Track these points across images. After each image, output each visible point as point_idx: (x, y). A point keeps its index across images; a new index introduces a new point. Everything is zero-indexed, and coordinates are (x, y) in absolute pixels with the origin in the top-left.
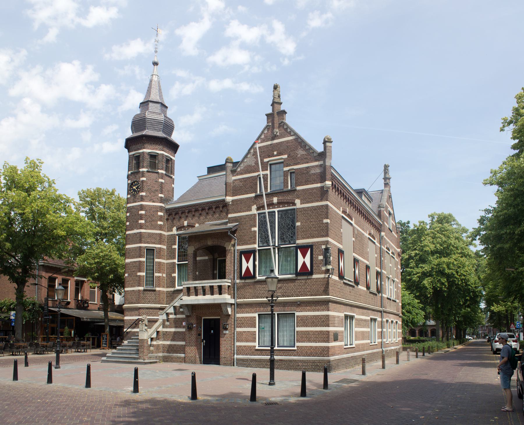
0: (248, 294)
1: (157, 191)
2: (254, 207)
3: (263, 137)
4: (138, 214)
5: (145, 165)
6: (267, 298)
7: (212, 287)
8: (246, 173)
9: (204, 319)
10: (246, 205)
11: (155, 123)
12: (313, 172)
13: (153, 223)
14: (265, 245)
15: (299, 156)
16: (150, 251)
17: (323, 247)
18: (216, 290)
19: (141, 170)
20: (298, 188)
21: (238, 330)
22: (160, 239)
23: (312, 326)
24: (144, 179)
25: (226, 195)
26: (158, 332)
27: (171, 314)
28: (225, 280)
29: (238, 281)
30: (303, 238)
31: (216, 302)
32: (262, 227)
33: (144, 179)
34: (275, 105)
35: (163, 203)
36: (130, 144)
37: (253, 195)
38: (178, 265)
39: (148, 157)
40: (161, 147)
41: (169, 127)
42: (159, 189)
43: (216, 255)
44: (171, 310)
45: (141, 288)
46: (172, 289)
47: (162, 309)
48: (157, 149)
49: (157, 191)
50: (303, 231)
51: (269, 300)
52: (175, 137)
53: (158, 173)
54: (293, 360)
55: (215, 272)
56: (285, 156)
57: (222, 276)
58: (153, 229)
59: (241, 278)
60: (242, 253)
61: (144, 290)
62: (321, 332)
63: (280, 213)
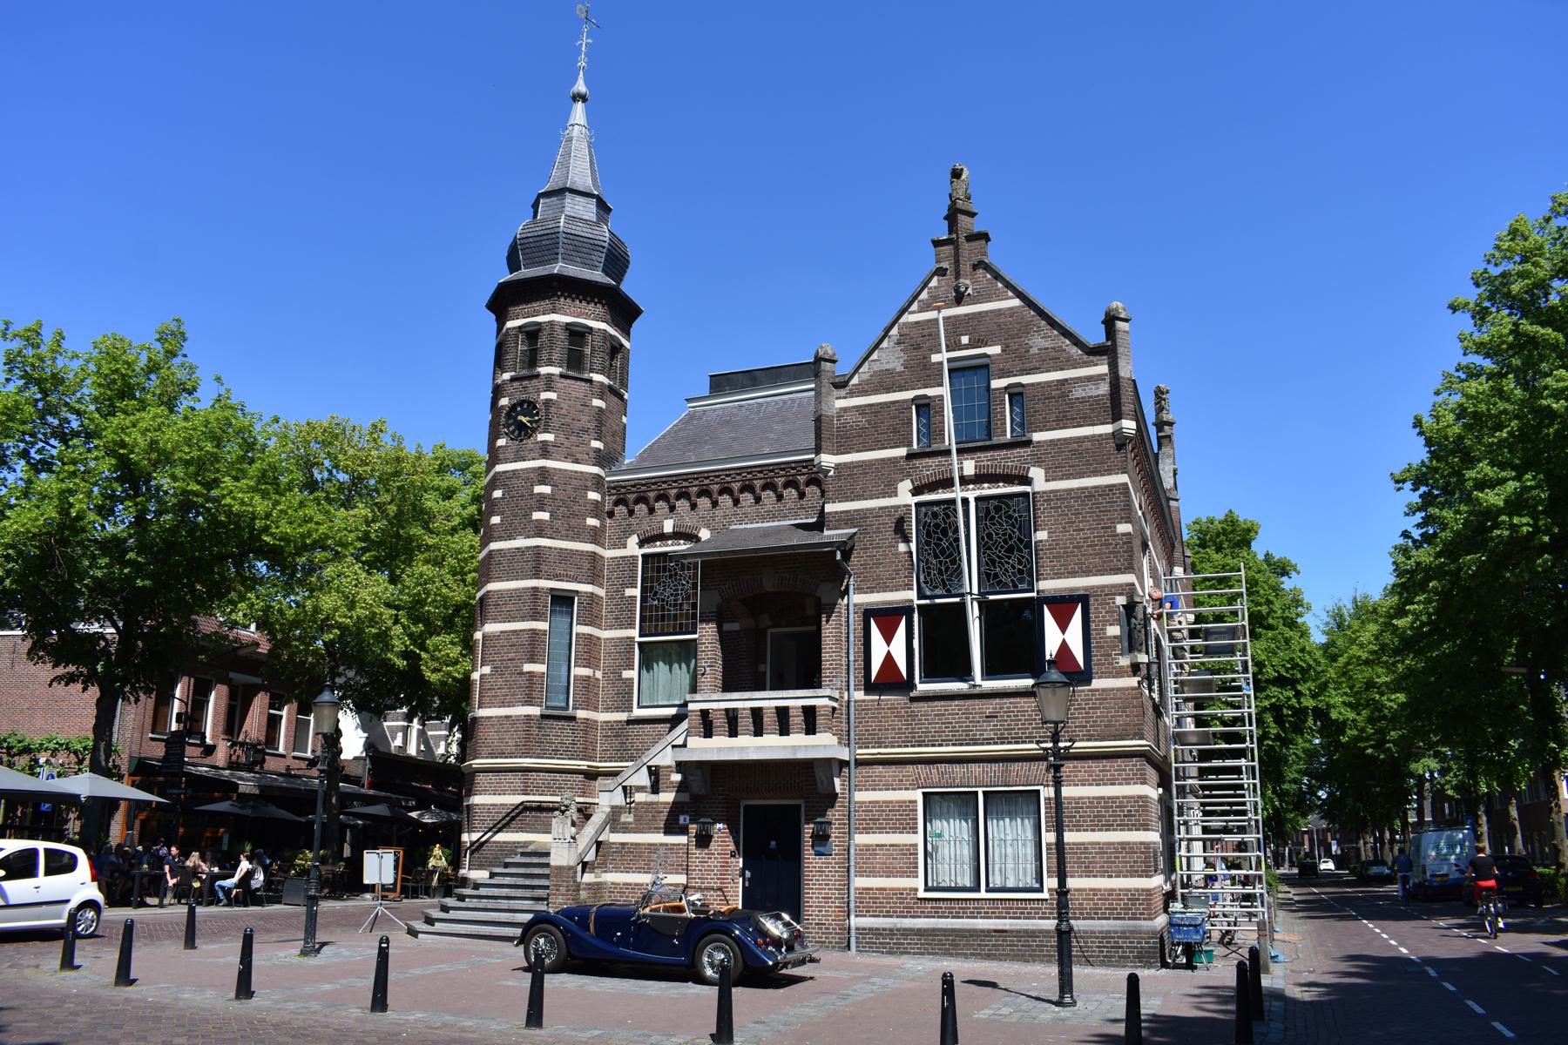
0: (891, 734)
1: (585, 431)
2: (905, 486)
3: (924, 295)
4: (532, 494)
5: (555, 356)
6: (1038, 742)
7: (757, 713)
8: (876, 391)
9: (746, 807)
10: (882, 478)
11: (580, 248)
12: (1078, 393)
13: (573, 522)
14: (938, 592)
15: (1034, 350)
16: (563, 601)
17: (1121, 600)
18: (797, 720)
19: (543, 370)
20: (1037, 437)
21: (860, 839)
22: (593, 568)
23: (1123, 827)
24: (552, 396)
25: (818, 451)
26: (599, 844)
27: (641, 789)
28: (819, 692)
29: (859, 695)
30: (1058, 575)
31: (801, 755)
32: (928, 543)
33: (552, 396)
34: (961, 217)
35: (602, 467)
36: (503, 301)
37: (902, 452)
38: (640, 644)
39: (562, 336)
40: (599, 309)
41: (616, 261)
42: (592, 425)
43: (766, 621)
44: (643, 778)
45: (535, 711)
46: (623, 716)
47: (615, 774)
48: (588, 317)
49: (585, 431)
50: (1058, 557)
51: (1045, 749)
52: (628, 287)
53: (590, 381)
54: (1041, 931)
55: (761, 668)
56: (995, 350)
57: (811, 678)
58: (572, 539)
59: (870, 688)
60: (869, 613)
61: (543, 717)
62: (1124, 845)
63: (983, 505)
